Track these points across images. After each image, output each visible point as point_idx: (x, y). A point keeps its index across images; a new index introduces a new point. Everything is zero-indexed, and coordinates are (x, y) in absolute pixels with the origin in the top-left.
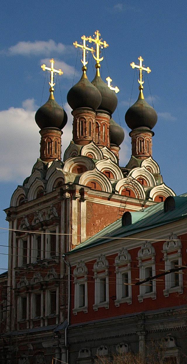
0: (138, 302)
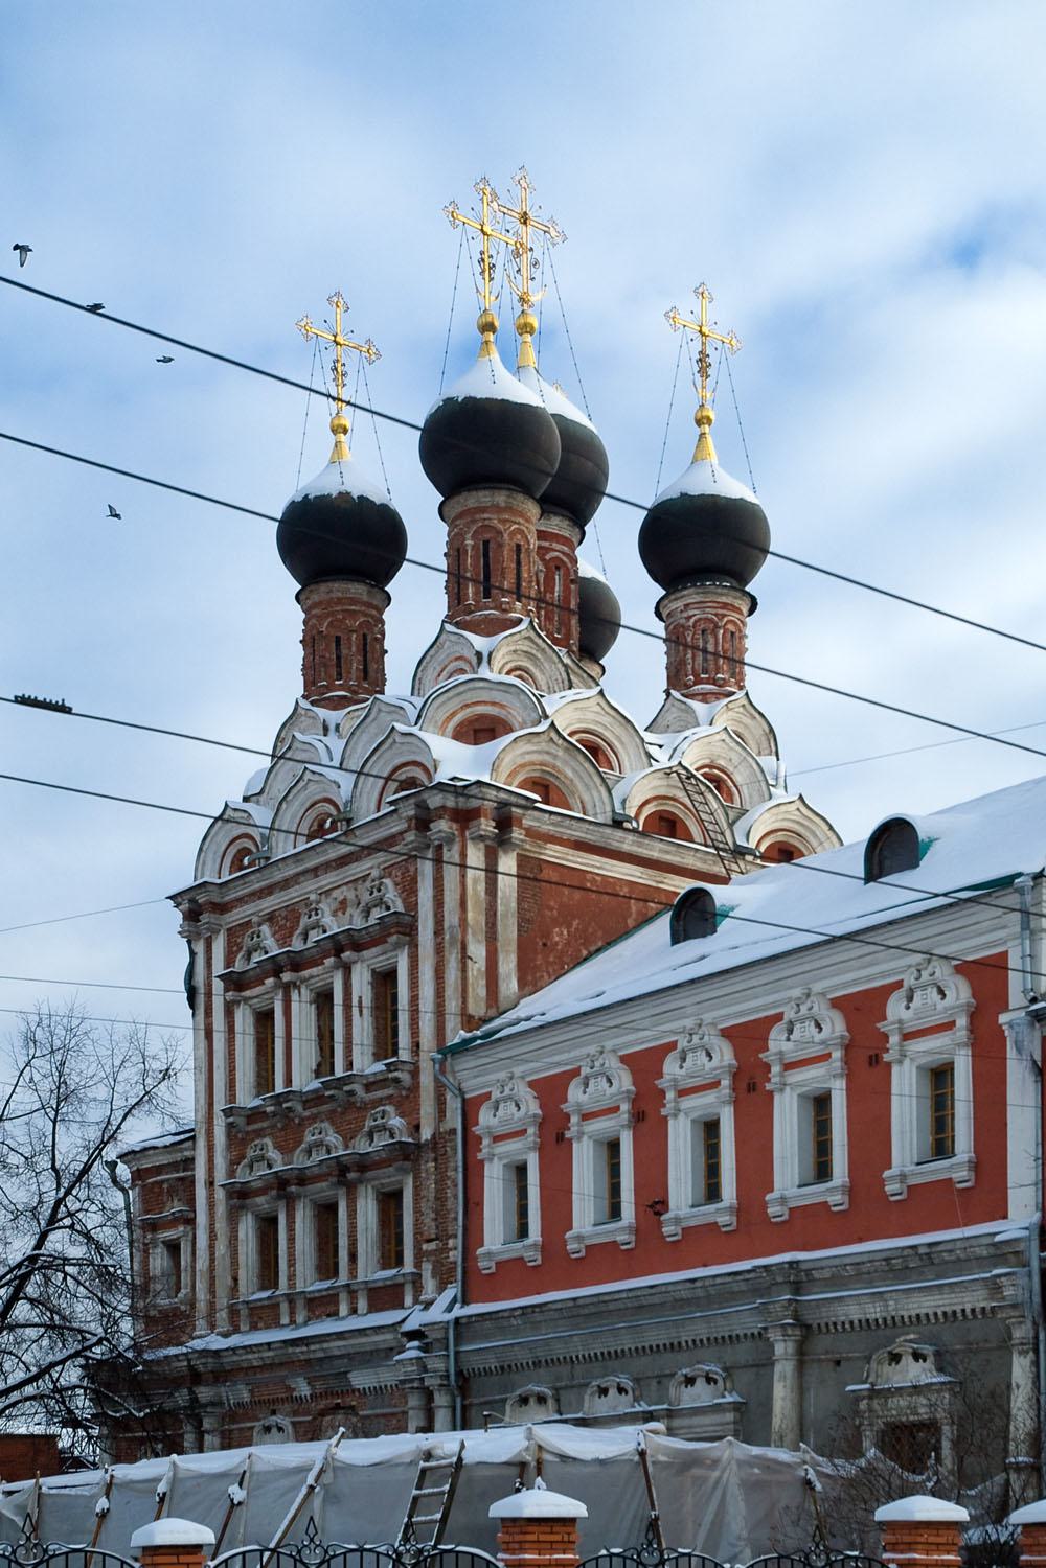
0: (568, 1255)
